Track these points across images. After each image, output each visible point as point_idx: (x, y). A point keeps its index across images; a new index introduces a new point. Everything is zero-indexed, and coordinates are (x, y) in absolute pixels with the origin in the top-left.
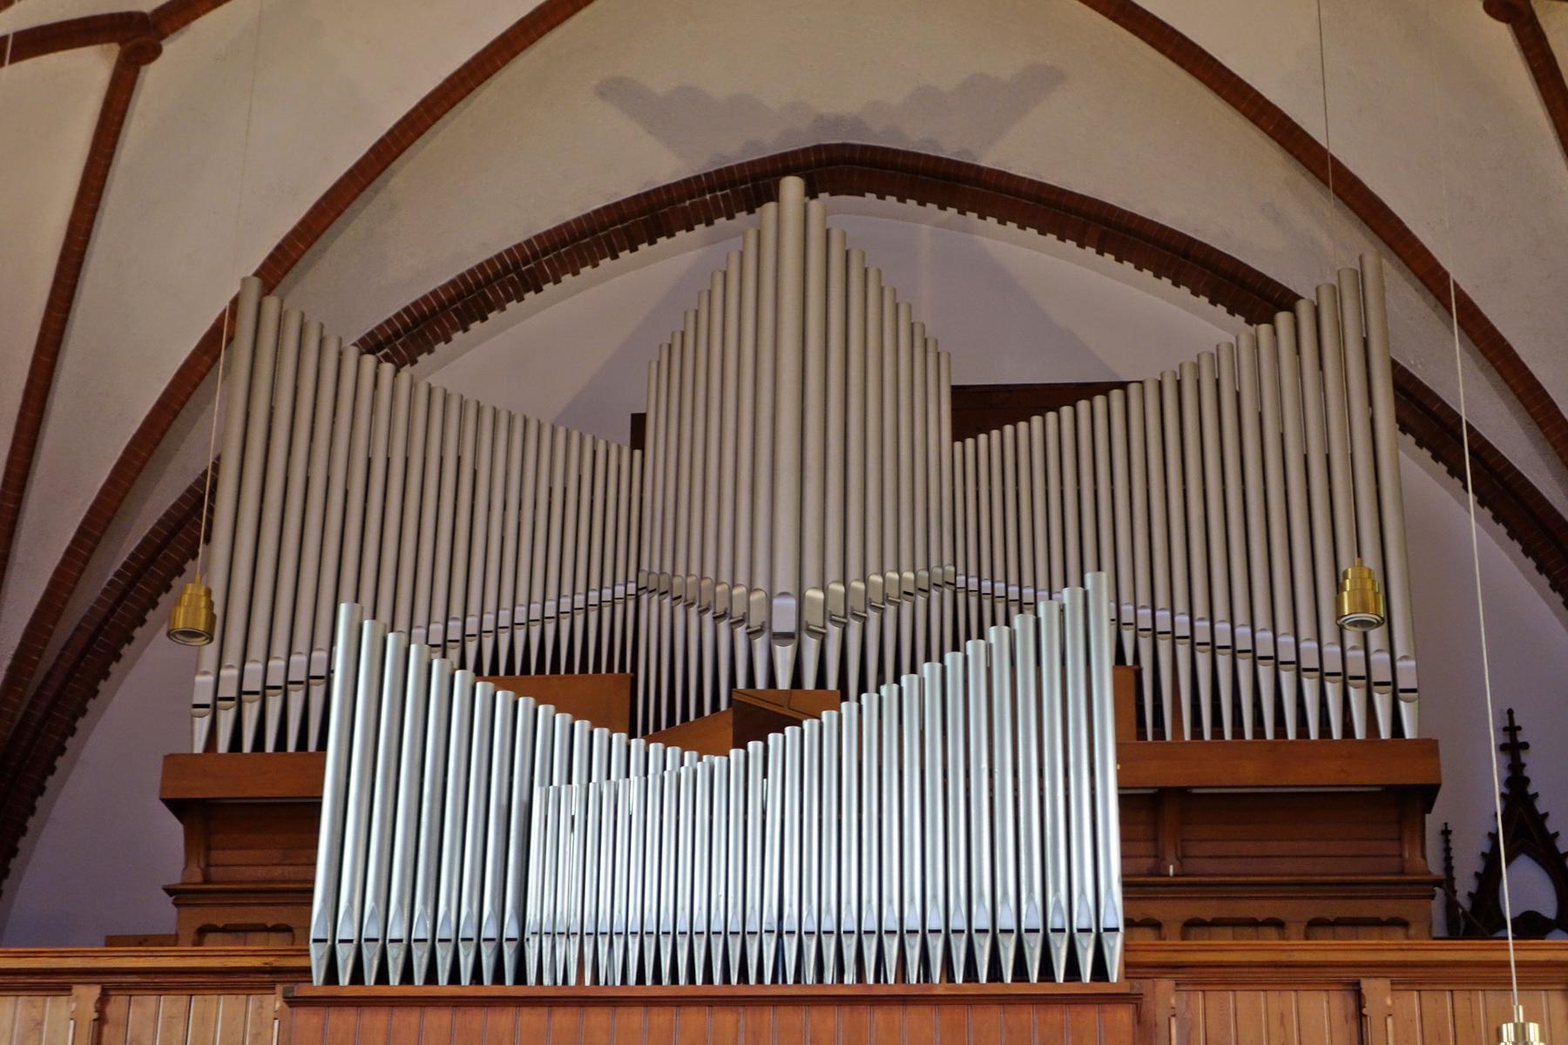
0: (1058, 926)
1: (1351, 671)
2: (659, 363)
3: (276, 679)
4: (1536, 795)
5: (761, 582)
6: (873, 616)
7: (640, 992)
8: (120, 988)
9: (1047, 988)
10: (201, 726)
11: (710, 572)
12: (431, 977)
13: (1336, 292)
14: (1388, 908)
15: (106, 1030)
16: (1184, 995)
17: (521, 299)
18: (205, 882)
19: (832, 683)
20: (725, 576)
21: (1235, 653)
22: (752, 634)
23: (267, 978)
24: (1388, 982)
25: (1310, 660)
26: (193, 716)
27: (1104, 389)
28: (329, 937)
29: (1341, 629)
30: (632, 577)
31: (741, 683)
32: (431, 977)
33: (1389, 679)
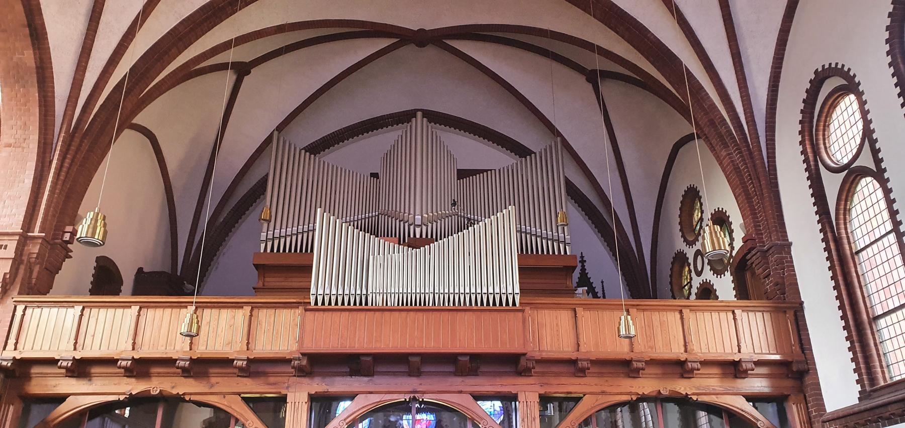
0: (504, 292)
1: (549, 238)
2: (384, 158)
3: (283, 234)
4: (588, 273)
5: (412, 212)
6: (430, 225)
7: (398, 308)
8: (256, 307)
9: (507, 308)
10: (263, 246)
11: (398, 209)
12: (343, 304)
13: (546, 150)
15: (252, 318)
16: (532, 311)
17: (338, 144)
18: (264, 286)
19: (434, 237)
20: (402, 211)
23: (297, 305)
24: (582, 309)
26: (261, 243)
27: (487, 171)
28: (316, 293)
29: (558, 226)
30: (377, 211)
31: (412, 236)
32: (343, 304)
33: (564, 240)
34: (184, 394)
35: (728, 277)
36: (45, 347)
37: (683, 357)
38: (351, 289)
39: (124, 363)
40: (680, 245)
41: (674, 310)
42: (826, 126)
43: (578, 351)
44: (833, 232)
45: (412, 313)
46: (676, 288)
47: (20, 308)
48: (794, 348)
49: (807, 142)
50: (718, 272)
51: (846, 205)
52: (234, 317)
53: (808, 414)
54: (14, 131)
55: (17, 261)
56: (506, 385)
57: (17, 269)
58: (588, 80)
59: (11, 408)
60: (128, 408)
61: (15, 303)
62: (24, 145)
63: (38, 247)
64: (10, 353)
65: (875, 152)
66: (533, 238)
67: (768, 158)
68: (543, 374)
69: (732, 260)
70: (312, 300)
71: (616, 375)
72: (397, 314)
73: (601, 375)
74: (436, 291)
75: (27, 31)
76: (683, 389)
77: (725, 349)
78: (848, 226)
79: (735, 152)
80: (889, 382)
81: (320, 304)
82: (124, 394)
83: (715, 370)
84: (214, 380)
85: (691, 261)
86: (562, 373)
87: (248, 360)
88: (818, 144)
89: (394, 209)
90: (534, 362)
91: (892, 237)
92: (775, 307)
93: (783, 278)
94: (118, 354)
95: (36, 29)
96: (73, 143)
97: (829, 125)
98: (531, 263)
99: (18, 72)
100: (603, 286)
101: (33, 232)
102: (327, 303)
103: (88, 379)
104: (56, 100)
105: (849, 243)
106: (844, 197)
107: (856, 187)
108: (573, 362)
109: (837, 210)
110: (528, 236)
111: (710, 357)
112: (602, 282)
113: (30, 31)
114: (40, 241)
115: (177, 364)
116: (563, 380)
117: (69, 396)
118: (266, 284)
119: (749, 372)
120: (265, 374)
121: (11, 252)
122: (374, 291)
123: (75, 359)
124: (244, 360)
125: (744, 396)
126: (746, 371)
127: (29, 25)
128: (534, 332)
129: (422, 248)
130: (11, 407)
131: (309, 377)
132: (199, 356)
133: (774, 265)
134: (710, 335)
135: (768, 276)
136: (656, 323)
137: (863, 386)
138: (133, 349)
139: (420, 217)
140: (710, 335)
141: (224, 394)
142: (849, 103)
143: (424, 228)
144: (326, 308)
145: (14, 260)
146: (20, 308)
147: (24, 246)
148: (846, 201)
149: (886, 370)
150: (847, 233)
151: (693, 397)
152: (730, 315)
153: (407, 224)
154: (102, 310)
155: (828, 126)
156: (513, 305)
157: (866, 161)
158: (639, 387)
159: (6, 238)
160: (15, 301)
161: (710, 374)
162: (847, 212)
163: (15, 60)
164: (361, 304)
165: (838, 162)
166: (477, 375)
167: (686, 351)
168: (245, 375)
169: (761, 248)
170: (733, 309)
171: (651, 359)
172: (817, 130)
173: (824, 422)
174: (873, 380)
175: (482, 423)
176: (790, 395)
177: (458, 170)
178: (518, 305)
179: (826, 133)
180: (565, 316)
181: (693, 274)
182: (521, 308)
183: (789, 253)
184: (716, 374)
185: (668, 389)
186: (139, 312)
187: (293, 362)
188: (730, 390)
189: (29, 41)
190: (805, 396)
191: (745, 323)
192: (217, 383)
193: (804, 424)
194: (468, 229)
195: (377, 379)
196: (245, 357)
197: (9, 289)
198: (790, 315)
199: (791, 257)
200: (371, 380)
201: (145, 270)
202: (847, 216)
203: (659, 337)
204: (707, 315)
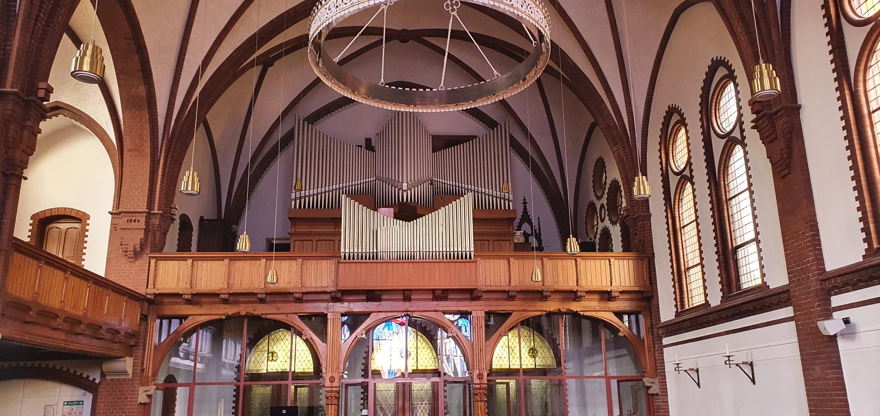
1: (502, 197)
10: (293, 203)
14: (506, 238)
21: (482, 193)
22: (399, 190)
25: (494, 195)
34: (262, 314)
38: (367, 248)
43: (510, 285)
44: (849, 85)
46: (589, 227)
51: (679, 196)
52: (291, 266)
55: (147, 230)
56: (464, 306)
63: (158, 220)
64: (151, 290)
65: (691, 171)
66: (487, 197)
68: (488, 299)
70: (342, 255)
71: (533, 300)
73: (525, 299)
74: (421, 250)
76: (574, 308)
78: (680, 209)
79: (622, 151)
80: (691, 307)
82: (224, 315)
83: (596, 297)
85: (598, 210)
91: (747, 192)
93: (644, 237)
96: (172, 147)
97: (676, 141)
98: (484, 215)
100: (539, 221)
106: (678, 192)
110: (483, 195)
111: (592, 289)
112: (539, 218)
114: (159, 216)
117: (188, 317)
122: (382, 250)
123: (193, 294)
125: (613, 312)
126: (615, 297)
131: (341, 302)
132: (271, 291)
134: (594, 274)
135: (636, 234)
136: (560, 268)
137: (677, 309)
139: (406, 184)
140: (594, 274)
141: (287, 314)
143: (409, 191)
144: (351, 259)
146: (153, 261)
147: (149, 219)
148: (680, 194)
149: (690, 300)
151: (580, 312)
152: (607, 261)
159: (138, 215)
160: (149, 257)
162: (680, 201)
163: (132, 92)
167: (577, 285)
170: (609, 258)
174: (683, 305)
175: (449, 329)
179: (674, 146)
180: (503, 263)
181: (599, 220)
182: (474, 260)
190: (651, 312)
198: (646, 261)
199: (650, 224)
201: (205, 218)
202: (680, 203)
204: (593, 261)
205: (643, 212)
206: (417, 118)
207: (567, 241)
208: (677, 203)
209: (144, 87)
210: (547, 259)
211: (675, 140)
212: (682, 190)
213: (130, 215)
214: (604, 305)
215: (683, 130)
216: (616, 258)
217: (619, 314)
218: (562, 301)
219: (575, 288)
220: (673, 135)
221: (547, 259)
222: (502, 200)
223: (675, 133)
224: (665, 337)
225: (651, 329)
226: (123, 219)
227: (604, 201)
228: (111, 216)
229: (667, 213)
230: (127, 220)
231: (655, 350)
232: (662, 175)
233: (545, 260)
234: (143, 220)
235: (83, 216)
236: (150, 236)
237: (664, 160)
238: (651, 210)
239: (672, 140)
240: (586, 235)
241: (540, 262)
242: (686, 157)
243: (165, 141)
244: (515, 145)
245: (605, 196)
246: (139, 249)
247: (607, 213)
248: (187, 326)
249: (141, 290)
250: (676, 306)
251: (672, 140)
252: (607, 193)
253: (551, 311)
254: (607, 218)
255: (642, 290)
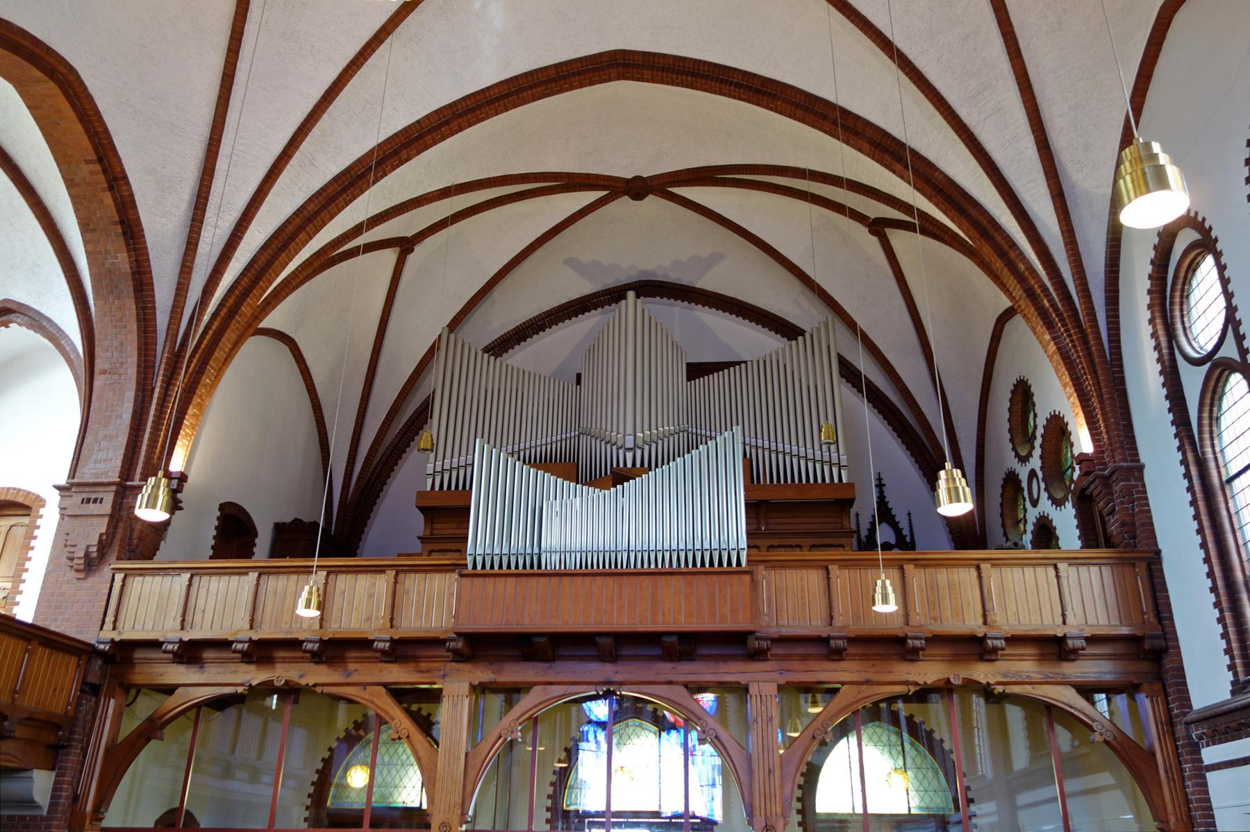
1: (824, 460)
3: (447, 467)
5: (621, 430)
7: (581, 571)
8: (402, 571)
10: (430, 481)
15: (398, 586)
18: (432, 534)
20: (609, 429)
22: (618, 449)
23: (452, 567)
27: (739, 363)
29: (821, 445)
31: (615, 466)
34: (315, 685)
35: (1069, 510)
36: (149, 626)
37: (980, 631)
38: (519, 543)
39: (239, 646)
40: (1014, 463)
41: (969, 566)
42: (1185, 297)
43: (831, 625)
45: (599, 579)
46: (1009, 522)
47: (119, 577)
48: (1146, 617)
49: (1158, 321)
50: (1058, 503)
51: (1211, 412)
52: (375, 584)
53: (1169, 711)
54: (109, 354)
56: (733, 672)
57: (115, 528)
58: (872, 232)
59: (112, 701)
60: (275, 696)
61: (114, 571)
62: (121, 371)
64: (108, 634)
65: (1240, 338)
67: (1110, 342)
68: (784, 658)
69: (1073, 486)
71: (886, 658)
72: (579, 579)
73: (865, 657)
75: (119, 229)
77: (1046, 622)
81: (479, 567)
82: (242, 685)
83: (1029, 650)
84: (352, 666)
85: (1024, 484)
86: (810, 655)
87: (392, 640)
88: (1173, 324)
89: (599, 426)
90: (769, 642)
92: (1120, 558)
93: (1133, 515)
94: (232, 635)
95: (129, 226)
99: (112, 281)
100: (910, 520)
101: (133, 480)
102: (488, 566)
103: (200, 665)
104: (158, 312)
105: (1218, 467)
106: (1208, 401)
107: (1225, 385)
108: (822, 641)
109: (1200, 419)
112: (909, 514)
113: (122, 228)
115: (304, 647)
116: (813, 665)
118: (435, 532)
119: (1080, 652)
120: (415, 659)
121: (107, 507)
124: (387, 641)
125: (1072, 686)
127: (122, 222)
128: (769, 600)
129: (637, 479)
130: (112, 701)
132: (331, 636)
133: (1119, 496)
135: (1112, 512)
137: (1236, 674)
138: (251, 627)
141: (365, 685)
142: (1209, 262)
145: (112, 516)
147: (123, 498)
148: (1212, 405)
150: (1214, 452)
153: (614, 447)
154: (214, 578)
155: (1188, 296)
156: (737, 565)
157: (1230, 351)
158: (920, 674)
159: (101, 489)
160: (113, 569)
161: (1023, 655)
162: (1214, 422)
164: (532, 566)
165: (1201, 348)
166: (694, 660)
167: (985, 623)
168: (389, 659)
169: (1100, 473)
170: (1054, 562)
171: (934, 636)
172: (1172, 304)
173: (1188, 723)
176: (1141, 684)
177: (688, 365)
178: (744, 563)
179: (1185, 307)
180: (814, 578)
182: (748, 569)
183: (1141, 479)
184: (1031, 655)
185: (961, 676)
186: (258, 580)
187: (447, 644)
188: (1052, 678)
189: (121, 242)
191: (1073, 581)
192: (356, 670)
193: (1162, 725)
194: (697, 448)
195: (559, 666)
196: (387, 637)
197: (106, 553)
198: (1141, 569)
199: (1144, 486)
200: (551, 666)
203: (946, 604)
205: (1125, 460)
206: (661, 324)
207: (936, 478)
208: (1206, 429)
209: (125, 254)
210: (912, 566)
211: (1185, 294)
212: (1217, 397)
213: (87, 489)
214: (1051, 669)
215: (1209, 262)
216: (1073, 561)
217: (1087, 691)
218: (950, 661)
219: (979, 630)
220: (1180, 281)
221: (912, 566)
222: (825, 467)
223: (1185, 278)
224: (1208, 745)
225: (1168, 724)
226: (74, 499)
227: (1035, 462)
228: (58, 492)
229: (1184, 454)
230: (81, 499)
231: (1183, 778)
232: (1158, 360)
233: (909, 568)
234: (109, 498)
235: (35, 500)
236: (120, 531)
237: (1163, 340)
238: (1143, 458)
239: (1178, 294)
240: (1005, 539)
241: (896, 573)
242: (1222, 302)
243: (166, 355)
244: (849, 372)
245: (1037, 452)
246: (95, 555)
247: (1043, 485)
248: (172, 707)
249: (90, 635)
250: (1232, 667)
251: (1178, 294)
252: (1041, 446)
253: (929, 682)
254: (1044, 495)
255: (1139, 633)
